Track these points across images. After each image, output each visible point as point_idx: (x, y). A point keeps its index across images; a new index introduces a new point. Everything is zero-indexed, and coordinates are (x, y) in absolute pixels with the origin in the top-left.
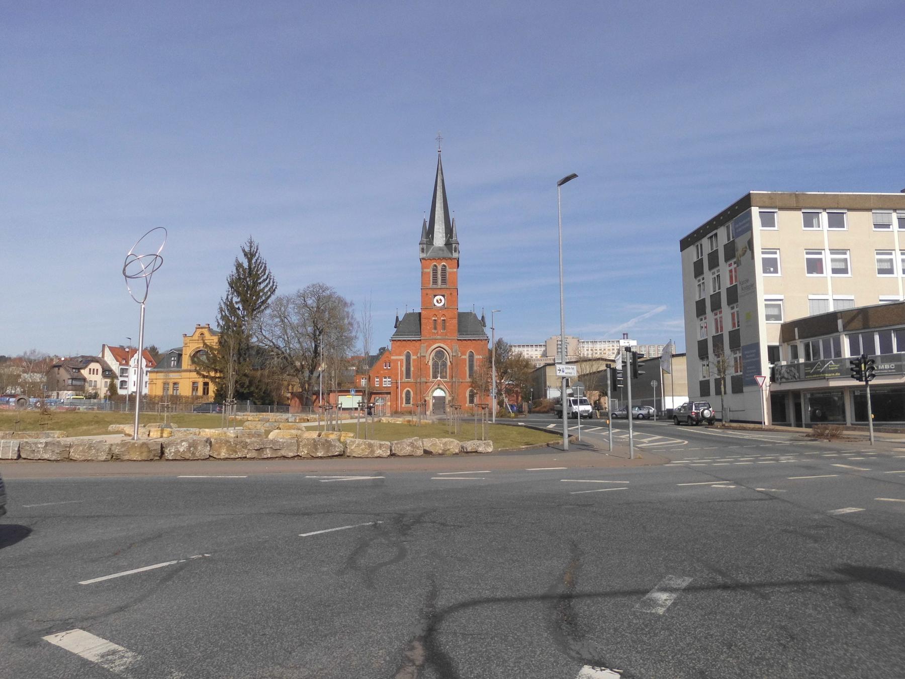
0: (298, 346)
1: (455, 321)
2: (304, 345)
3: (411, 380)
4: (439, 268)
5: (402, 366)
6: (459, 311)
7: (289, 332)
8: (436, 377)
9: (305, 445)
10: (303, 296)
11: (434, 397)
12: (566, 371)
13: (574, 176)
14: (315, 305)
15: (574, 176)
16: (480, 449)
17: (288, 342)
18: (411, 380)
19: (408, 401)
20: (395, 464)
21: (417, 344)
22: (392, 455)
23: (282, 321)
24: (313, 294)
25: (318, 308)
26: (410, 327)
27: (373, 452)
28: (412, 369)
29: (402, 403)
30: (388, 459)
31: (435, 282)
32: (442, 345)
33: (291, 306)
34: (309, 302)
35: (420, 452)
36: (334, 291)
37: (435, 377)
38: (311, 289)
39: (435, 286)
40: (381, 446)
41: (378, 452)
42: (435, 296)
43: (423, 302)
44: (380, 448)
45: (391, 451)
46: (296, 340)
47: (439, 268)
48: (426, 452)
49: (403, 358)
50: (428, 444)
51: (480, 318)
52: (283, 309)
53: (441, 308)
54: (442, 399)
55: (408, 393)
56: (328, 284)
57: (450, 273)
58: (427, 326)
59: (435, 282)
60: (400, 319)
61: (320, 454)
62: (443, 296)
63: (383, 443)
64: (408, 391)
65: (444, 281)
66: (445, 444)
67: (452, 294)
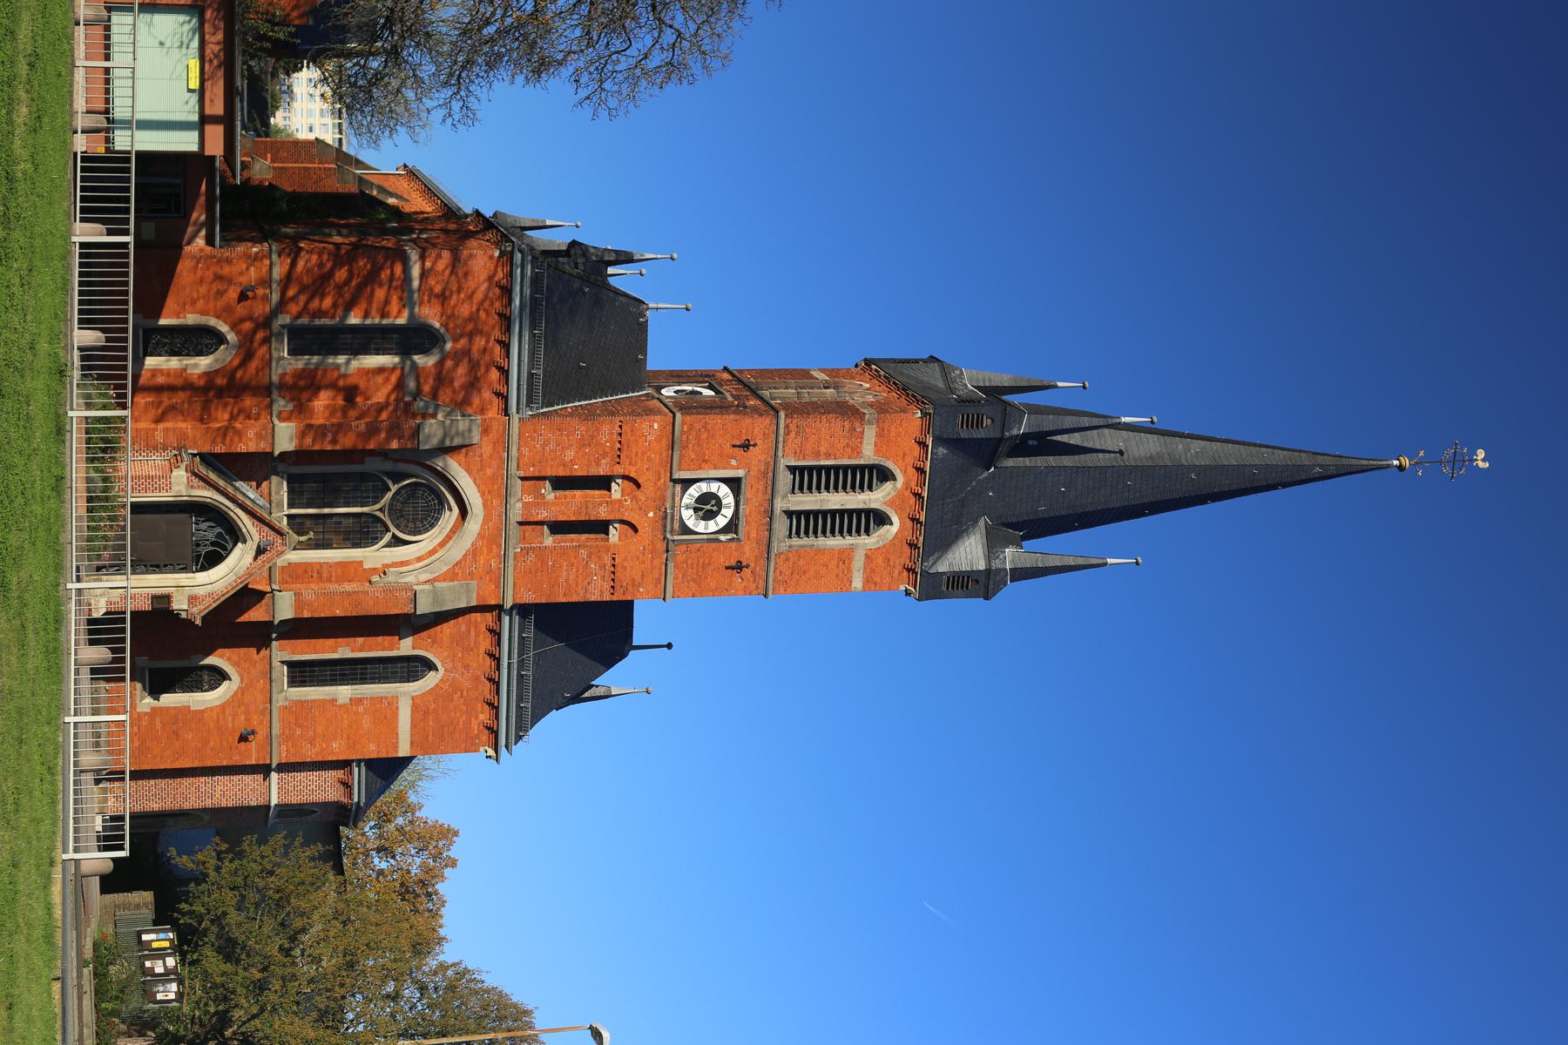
4: (876, 498)
31: (807, 477)
42: (734, 484)
47: (876, 498)
57: (845, 556)
59: (807, 477)
65: (808, 522)
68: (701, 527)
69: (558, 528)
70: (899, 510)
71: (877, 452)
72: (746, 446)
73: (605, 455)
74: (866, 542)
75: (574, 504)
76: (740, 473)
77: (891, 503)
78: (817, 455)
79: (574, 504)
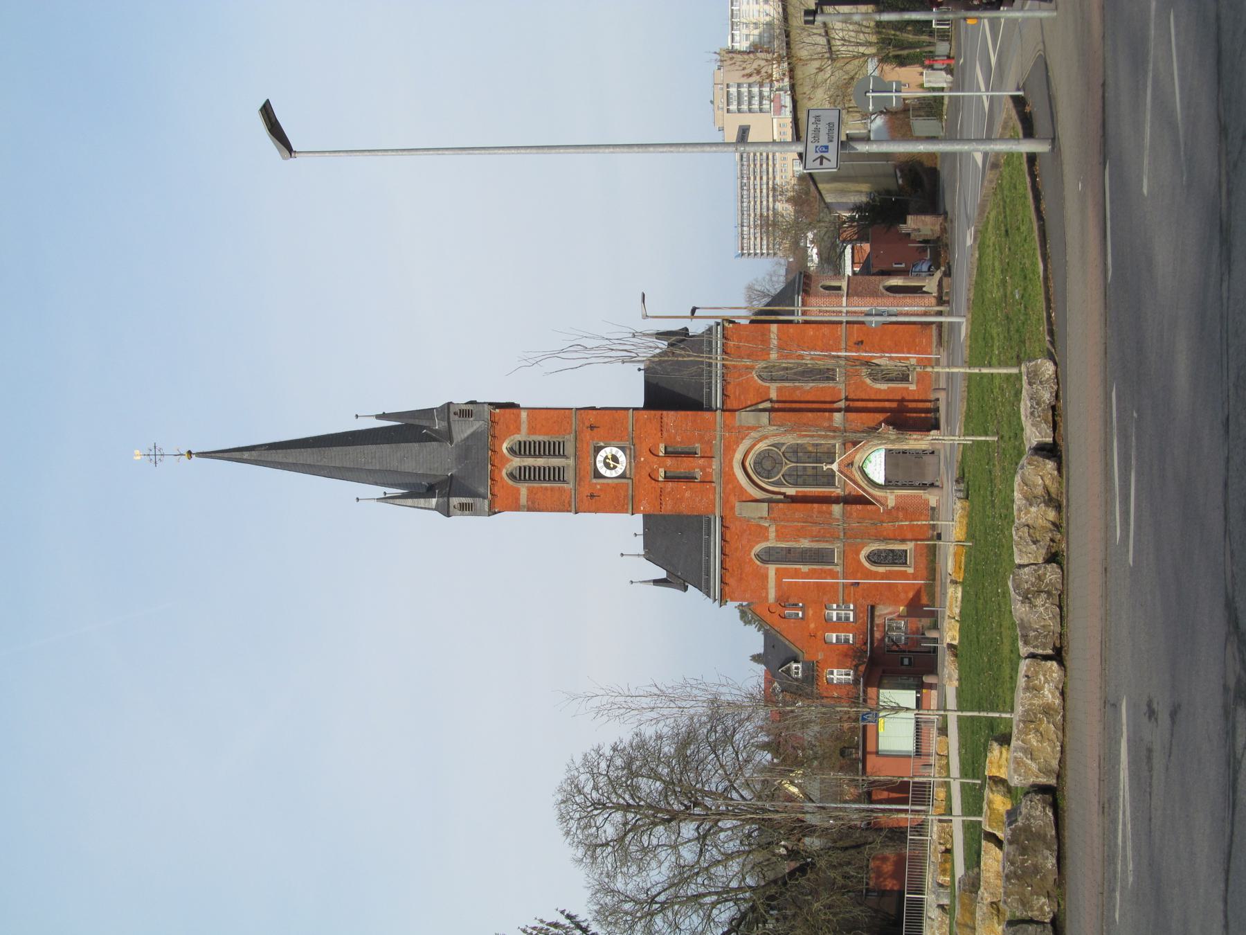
0: (734, 866)
1: (670, 417)
2: (732, 846)
3: (837, 548)
4: (517, 462)
5: (797, 574)
6: (640, 403)
7: (692, 890)
8: (831, 474)
9: (1024, 903)
10: (593, 848)
11: (889, 484)
12: (824, 141)
13: (267, 111)
14: (618, 816)
15: (267, 111)
16: (1047, 396)
17: (725, 894)
18: (837, 548)
19: (898, 558)
20: (1083, 650)
21: (734, 527)
22: (1058, 656)
23: (664, 906)
24: (587, 822)
25: (627, 808)
26: (679, 550)
27: (1047, 710)
28: (805, 544)
29: (904, 575)
30: (1067, 664)
31: (556, 475)
32: (738, 456)
33: (619, 884)
34: (610, 832)
35: (1052, 574)
36: (579, 761)
37: (829, 478)
38: (573, 825)
39: (570, 475)
40: (1033, 689)
41: (1049, 695)
42: (597, 475)
43: (617, 507)
44: (1037, 689)
45: (1046, 658)
46: (720, 870)
47: (517, 462)
48: (1053, 558)
49: (772, 569)
50: (1026, 554)
51: (663, 345)
52: (627, 906)
53: (633, 457)
54: (892, 458)
55: (875, 558)
56: (559, 777)
57: (532, 430)
58: (686, 500)
60: (662, 574)
61: (1051, 863)
62: (598, 450)
63: (1021, 681)
64: (868, 558)
65: (554, 449)
66: (1030, 500)
67: (597, 423)
68: (615, 450)
69: (691, 454)
70: (503, 455)
71: (518, 490)
72: (592, 496)
73: (669, 493)
74: (522, 436)
75: (683, 466)
76: (594, 481)
77: (508, 460)
78: (552, 489)
79: (683, 466)
